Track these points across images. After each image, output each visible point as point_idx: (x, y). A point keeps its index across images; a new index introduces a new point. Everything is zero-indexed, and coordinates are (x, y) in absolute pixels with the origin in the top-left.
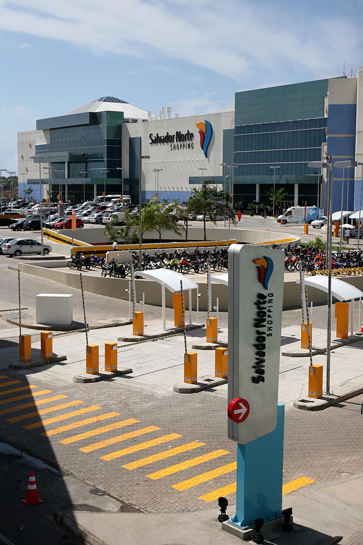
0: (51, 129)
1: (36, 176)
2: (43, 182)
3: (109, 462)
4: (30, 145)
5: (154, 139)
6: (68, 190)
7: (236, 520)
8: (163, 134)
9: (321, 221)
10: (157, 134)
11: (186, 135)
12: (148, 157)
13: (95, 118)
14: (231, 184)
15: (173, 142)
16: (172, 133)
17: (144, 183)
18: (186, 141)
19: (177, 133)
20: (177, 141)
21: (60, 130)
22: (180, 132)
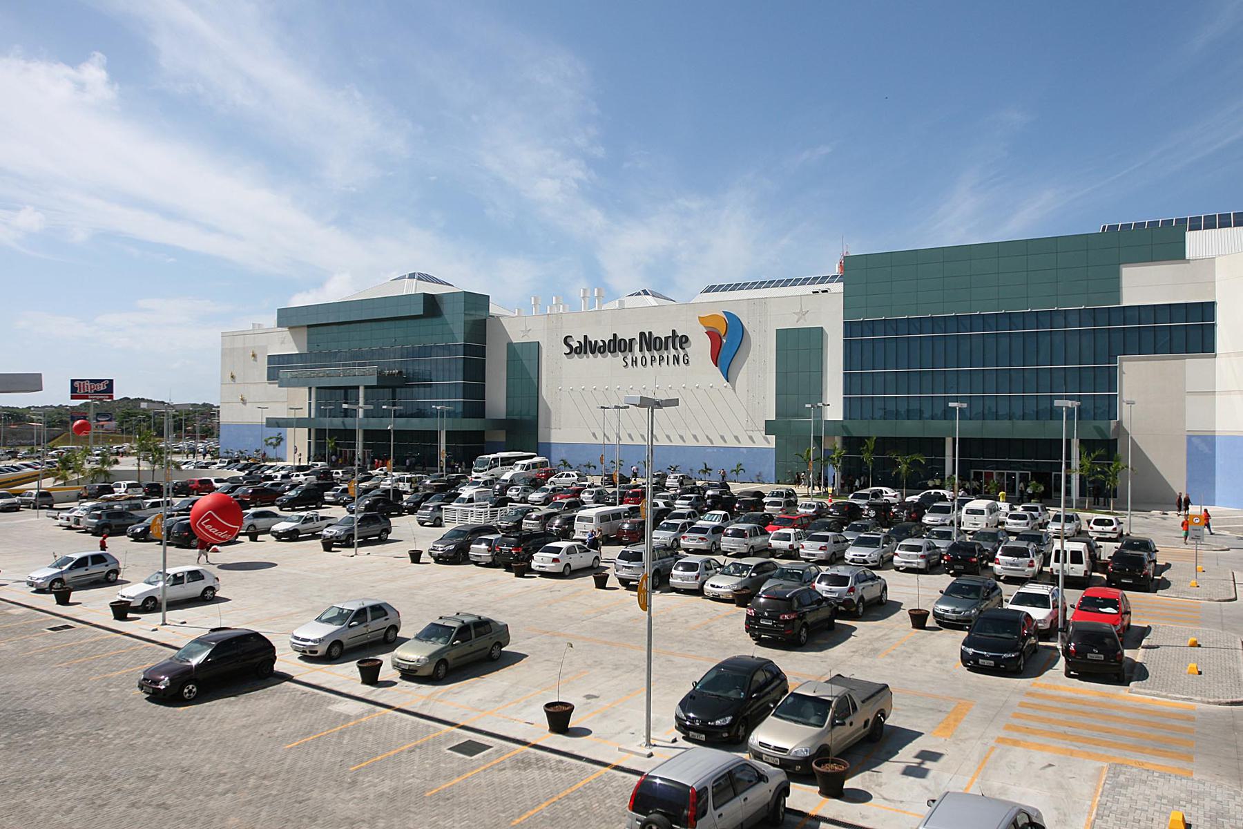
0: (309, 326)
1: (282, 413)
2: (299, 423)
3: (696, 821)
4: (254, 355)
5: (575, 345)
6: (365, 439)
7: (1089, 522)
8: (601, 335)
9: (700, 523)
10: (586, 337)
11: (667, 338)
12: (674, 402)
13: (432, 305)
14: (1068, 492)
15: (631, 351)
16: (628, 332)
17: (548, 427)
18: (666, 349)
19: (642, 334)
20: (641, 350)
21: (334, 327)
22: (650, 333)
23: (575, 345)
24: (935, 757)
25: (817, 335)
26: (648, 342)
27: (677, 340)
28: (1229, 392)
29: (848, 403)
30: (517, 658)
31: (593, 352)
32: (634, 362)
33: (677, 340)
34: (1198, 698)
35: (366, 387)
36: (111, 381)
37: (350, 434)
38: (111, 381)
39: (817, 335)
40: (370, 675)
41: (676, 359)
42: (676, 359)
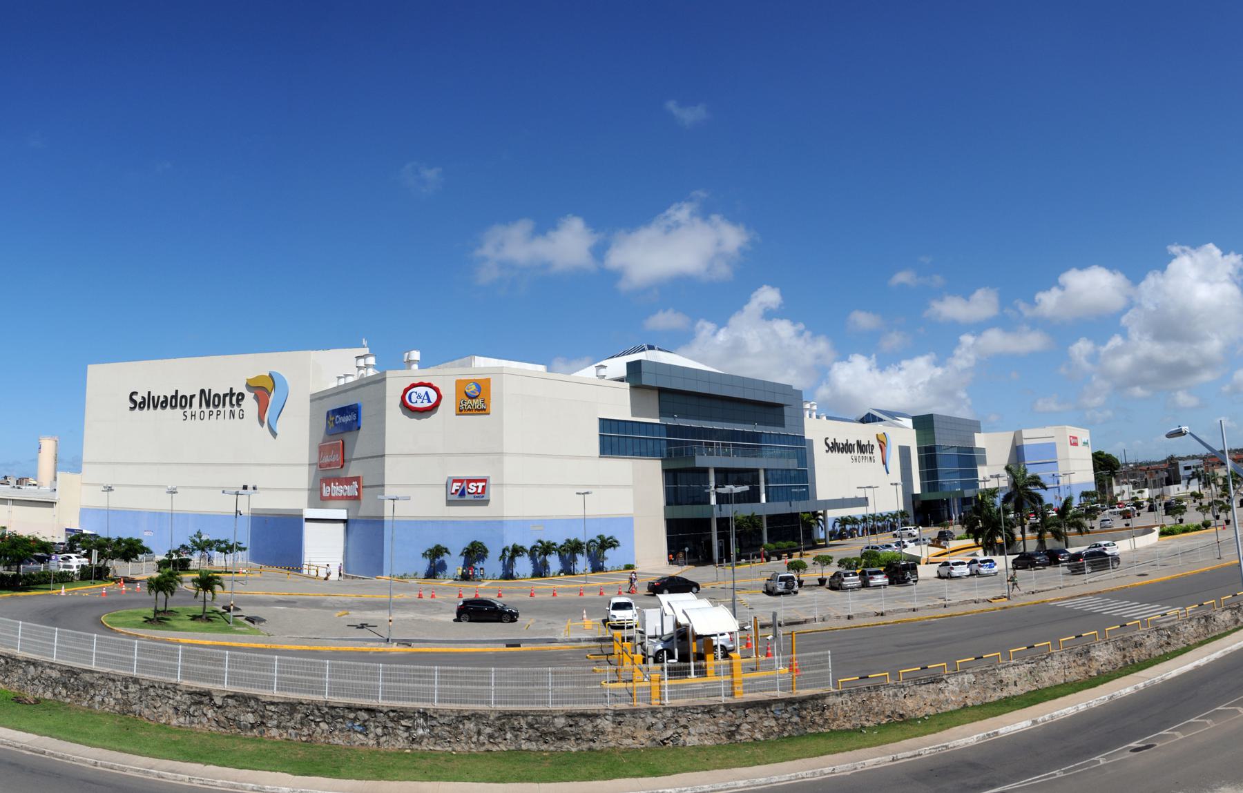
8: (883, 468)
11: (225, 395)
19: (202, 391)
23: (138, 399)
24: (432, 574)
25: (908, 448)
26: (208, 398)
27: (234, 399)
28: (625, 486)
29: (922, 485)
30: (424, 555)
31: (155, 407)
32: (193, 415)
33: (234, 399)
34: (584, 644)
35: (717, 471)
36: (603, 422)
37: (705, 523)
38: (603, 422)
39: (908, 448)
40: (733, 650)
41: (232, 414)
42: (232, 414)
